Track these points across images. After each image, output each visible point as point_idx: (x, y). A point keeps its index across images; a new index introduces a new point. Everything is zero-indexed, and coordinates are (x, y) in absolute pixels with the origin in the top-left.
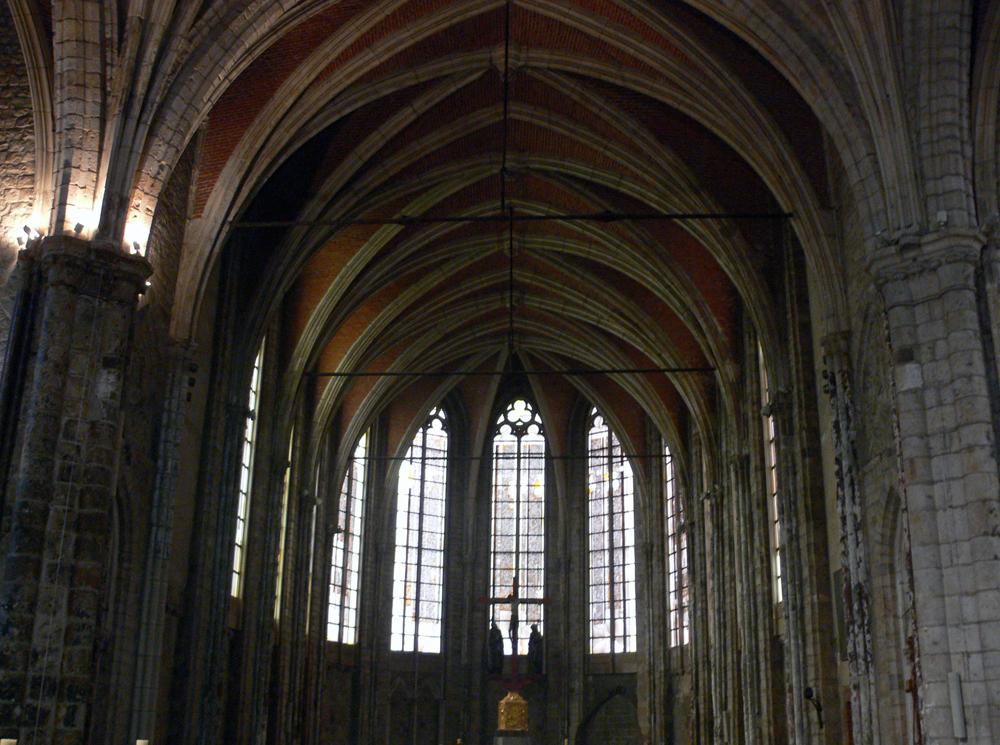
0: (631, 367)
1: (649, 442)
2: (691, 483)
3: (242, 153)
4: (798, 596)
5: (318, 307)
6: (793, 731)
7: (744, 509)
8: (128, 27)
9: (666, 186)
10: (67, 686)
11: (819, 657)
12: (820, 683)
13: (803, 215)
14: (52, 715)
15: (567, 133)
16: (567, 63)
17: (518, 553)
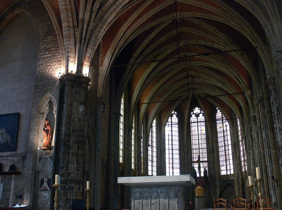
0: (224, 94)
1: (232, 115)
2: (244, 126)
3: (111, 49)
4: (269, 152)
5: (137, 86)
6: (271, 189)
7: (256, 130)
8: (79, 22)
9: (225, 44)
10: (78, 181)
11: (276, 168)
12: (277, 175)
13: (259, 47)
14: (75, 188)
15: (197, 33)
16: (194, 15)
17: (199, 149)
